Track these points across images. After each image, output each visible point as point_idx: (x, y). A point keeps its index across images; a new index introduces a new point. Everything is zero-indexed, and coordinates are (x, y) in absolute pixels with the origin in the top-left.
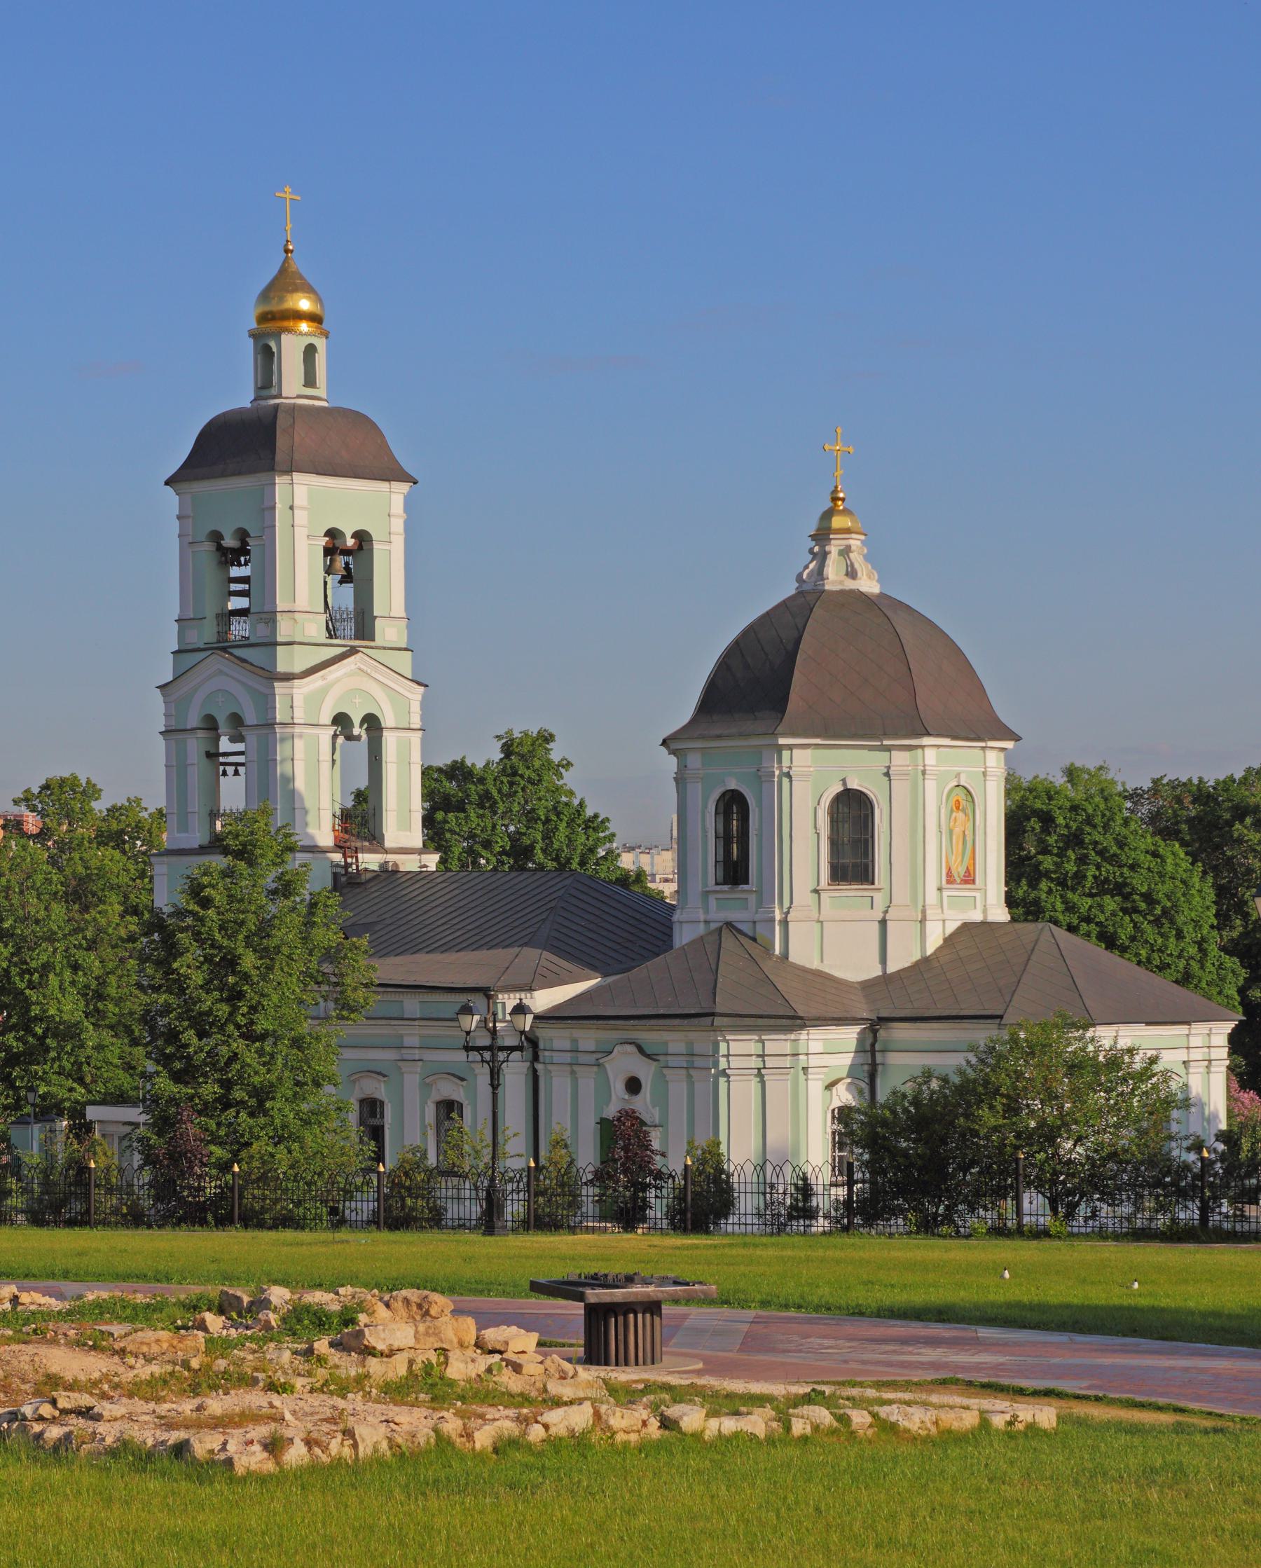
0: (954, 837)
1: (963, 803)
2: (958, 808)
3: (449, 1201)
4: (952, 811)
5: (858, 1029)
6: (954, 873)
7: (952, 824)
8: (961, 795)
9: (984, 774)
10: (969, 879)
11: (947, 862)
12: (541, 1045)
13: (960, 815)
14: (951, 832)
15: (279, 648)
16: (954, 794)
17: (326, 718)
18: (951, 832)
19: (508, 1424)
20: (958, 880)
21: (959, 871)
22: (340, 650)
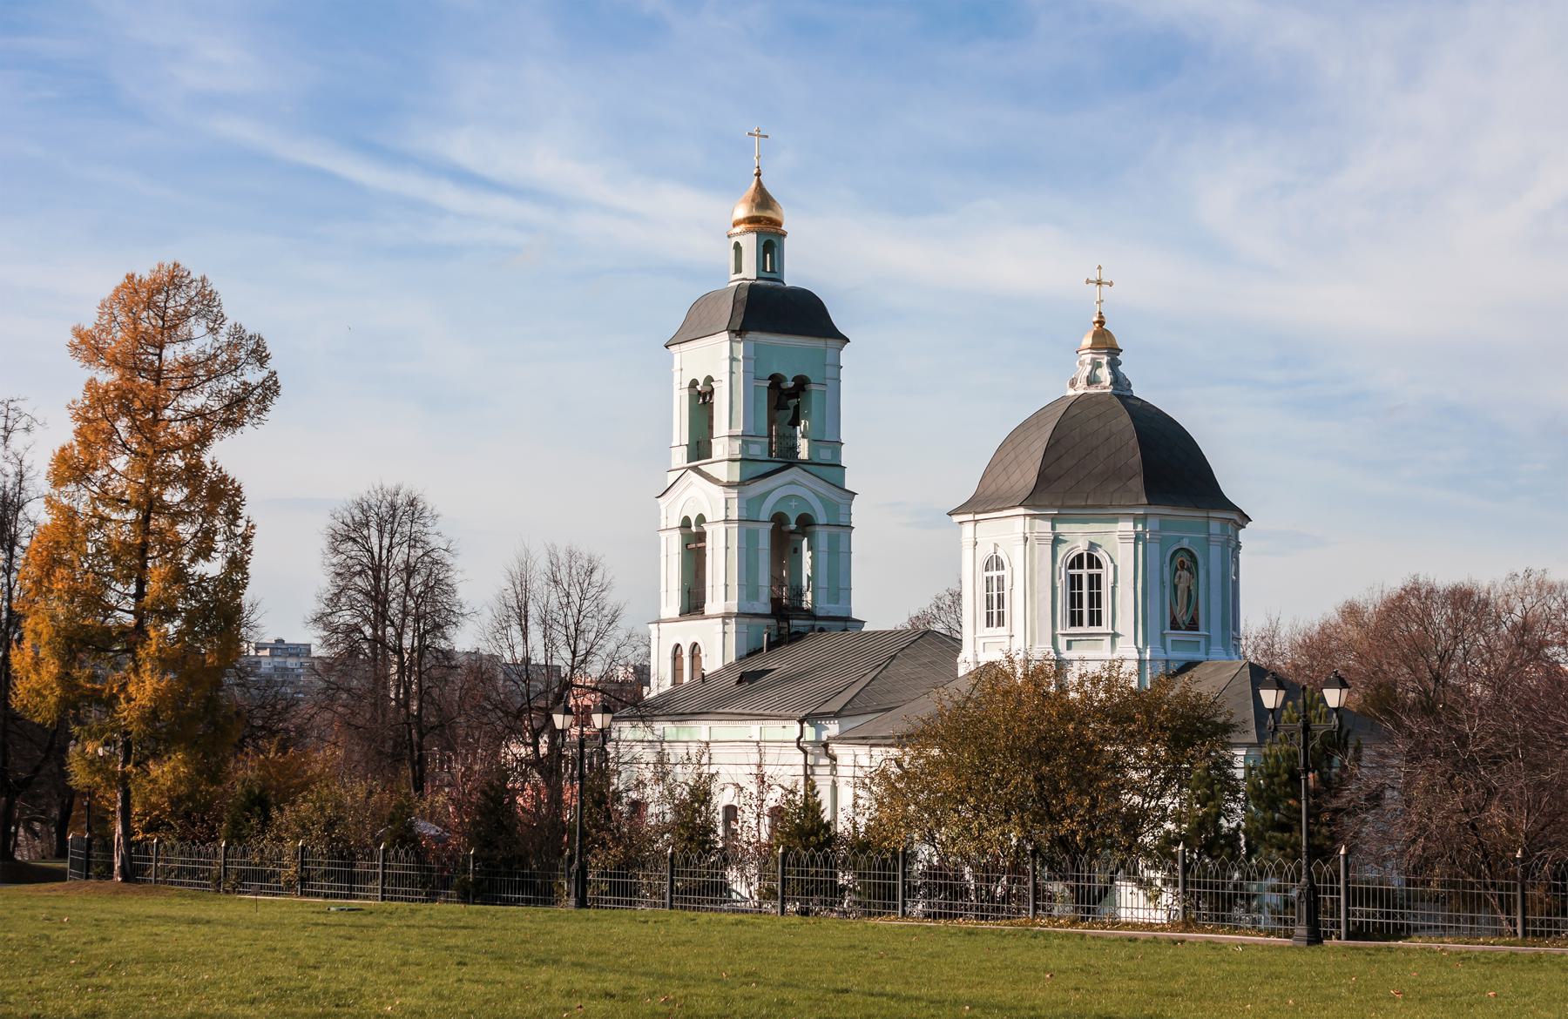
0: (1179, 593)
1: (1187, 563)
2: (1182, 568)
3: (1141, 906)
4: (1177, 570)
5: (1262, 692)
6: (1179, 620)
7: (1176, 580)
8: (1186, 559)
9: (1207, 540)
10: (1193, 625)
11: (1172, 612)
12: (795, 744)
13: (1185, 574)
14: (1176, 587)
15: (740, 456)
16: (1178, 555)
17: (678, 523)
18: (1176, 587)
19: (348, 618)
20: (1183, 627)
21: (1183, 618)
22: (780, 465)
